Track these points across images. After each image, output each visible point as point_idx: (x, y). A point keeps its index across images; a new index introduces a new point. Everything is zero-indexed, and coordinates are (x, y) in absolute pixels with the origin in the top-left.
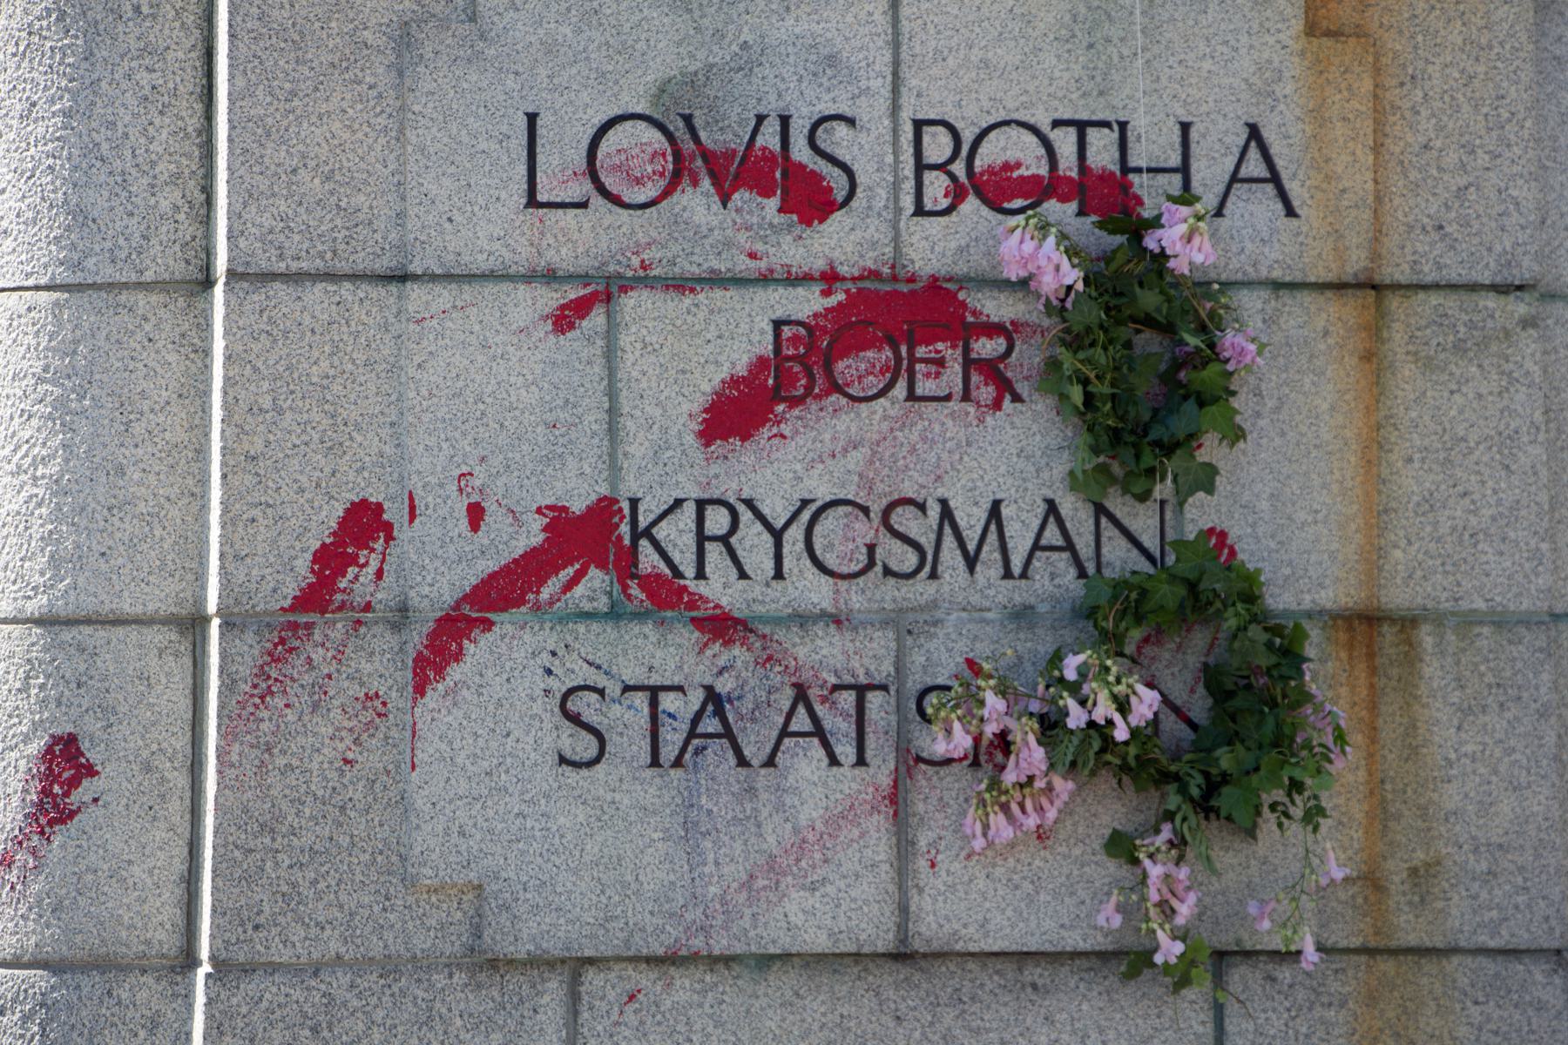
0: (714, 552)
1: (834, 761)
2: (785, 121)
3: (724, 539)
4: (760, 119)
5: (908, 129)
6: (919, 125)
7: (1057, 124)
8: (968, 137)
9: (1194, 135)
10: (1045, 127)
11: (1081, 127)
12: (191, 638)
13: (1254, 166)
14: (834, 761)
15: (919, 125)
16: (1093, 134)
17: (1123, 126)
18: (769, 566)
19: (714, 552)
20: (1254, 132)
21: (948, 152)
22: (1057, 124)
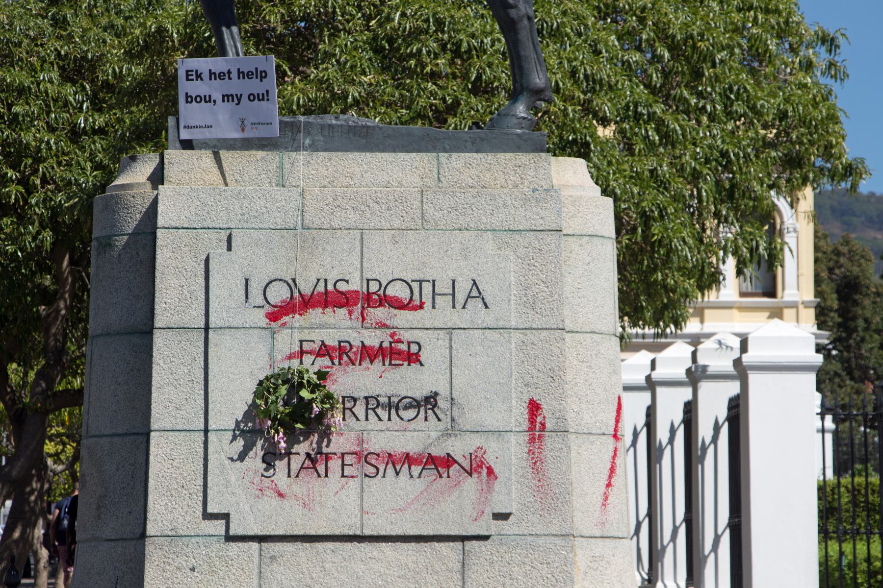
0: (370, 412)
1: (319, 476)
2: (326, 281)
3: (351, 409)
4: (318, 280)
5: (365, 281)
6: (368, 280)
7: (413, 281)
8: (384, 285)
9: (456, 283)
10: (409, 281)
11: (421, 282)
12: (830, 584)
13: (475, 293)
14: (319, 476)
15: (368, 280)
16: (424, 284)
17: (434, 281)
18: (364, 418)
19: (370, 412)
20: (475, 283)
21: (377, 288)
22: (413, 281)
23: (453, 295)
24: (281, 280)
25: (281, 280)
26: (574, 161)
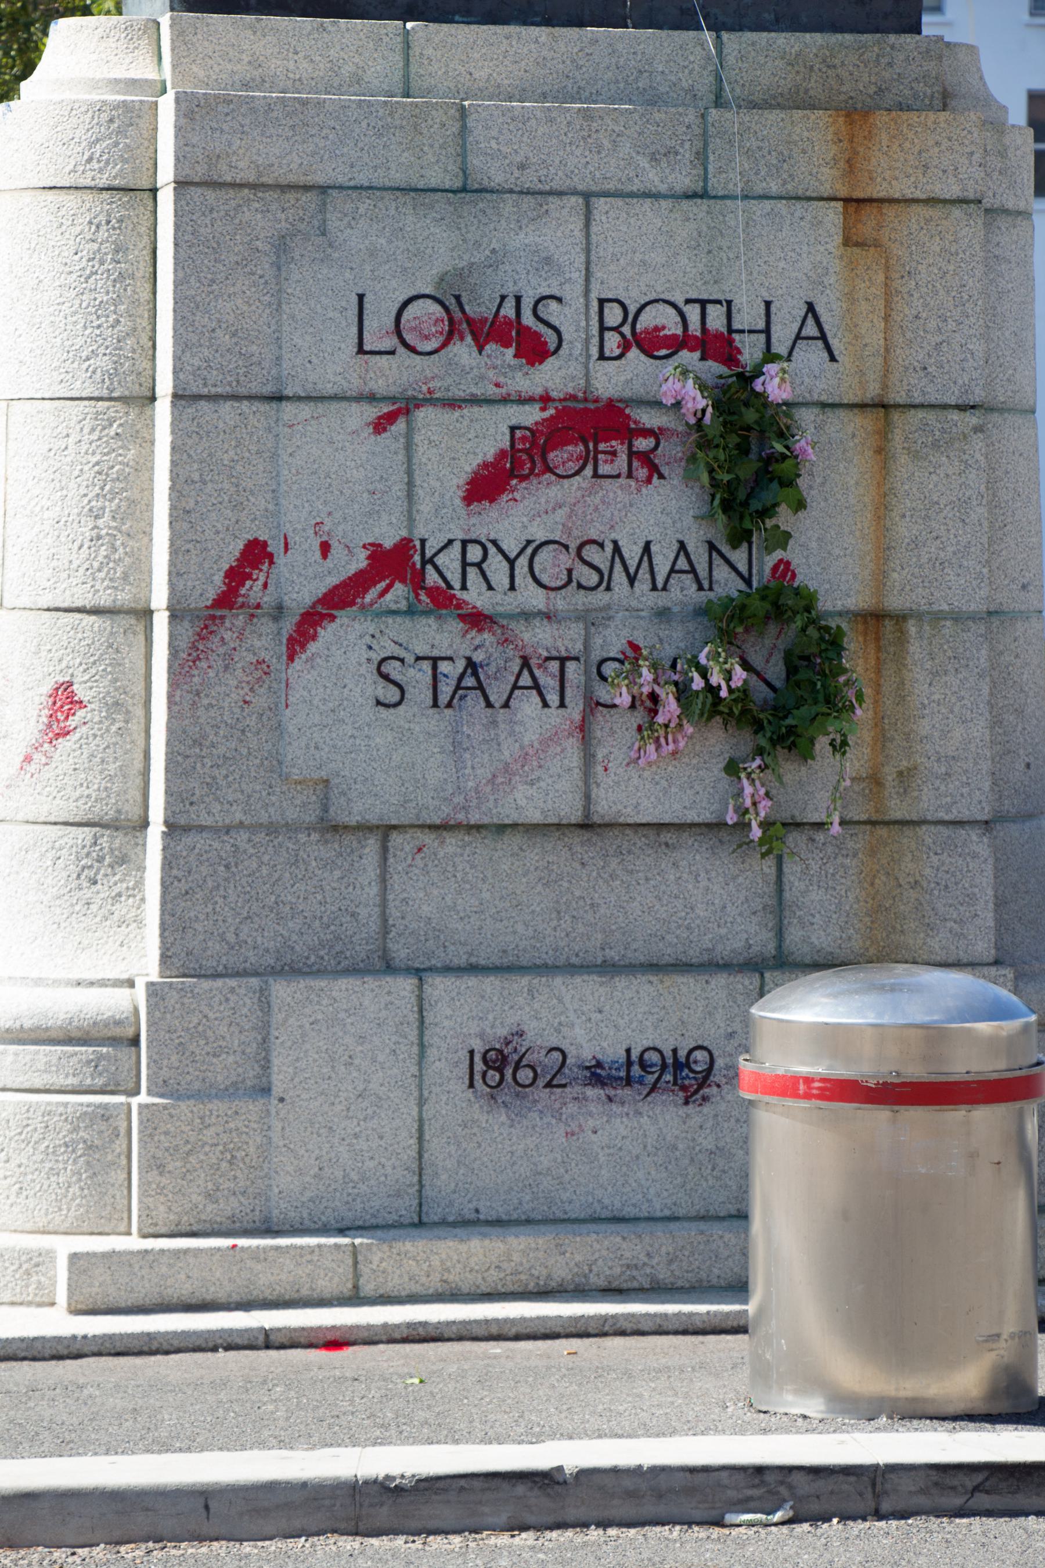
0: (472, 573)
1: (545, 705)
2: (518, 299)
3: (479, 565)
4: (503, 298)
5: (595, 305)
6: (602, 302)
7: (688, 301)
8: (632, 309)
10: (681, 304)
11: (703, 303)
13: (810, 329)
14: (545, 705)
15: (602, 302)
16: (710, 308)
17: (729, 303)
18: (506, 581)
19: (472, 573)
20: (811, 308)
21: (620, 319)
22: (688, 301)
23: (767, 331)
24: (656, 301)
25: (656, 301)
26: (669, 36)
